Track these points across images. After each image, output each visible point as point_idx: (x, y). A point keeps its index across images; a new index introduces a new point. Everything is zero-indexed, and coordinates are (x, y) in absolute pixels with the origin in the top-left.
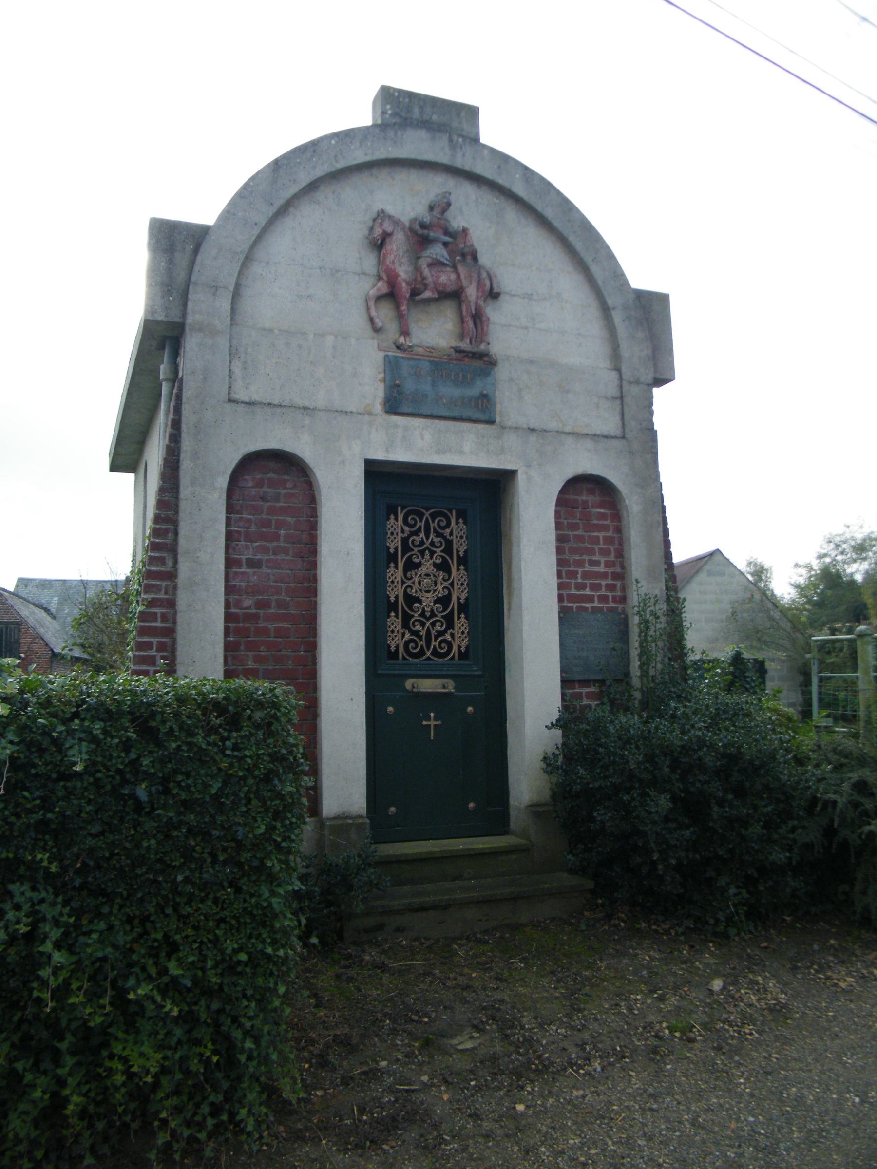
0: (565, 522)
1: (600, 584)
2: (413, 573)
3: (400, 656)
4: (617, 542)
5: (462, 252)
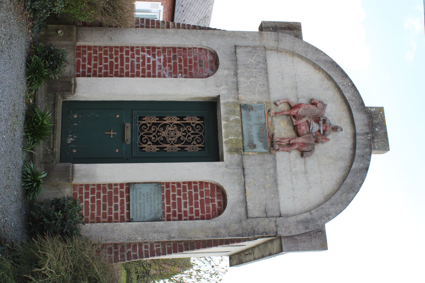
0: (204, 190)
1: (175, 208)
2: (176, 128)
3: (140, 122)
4: (197, 217)
5: (320, 137)
